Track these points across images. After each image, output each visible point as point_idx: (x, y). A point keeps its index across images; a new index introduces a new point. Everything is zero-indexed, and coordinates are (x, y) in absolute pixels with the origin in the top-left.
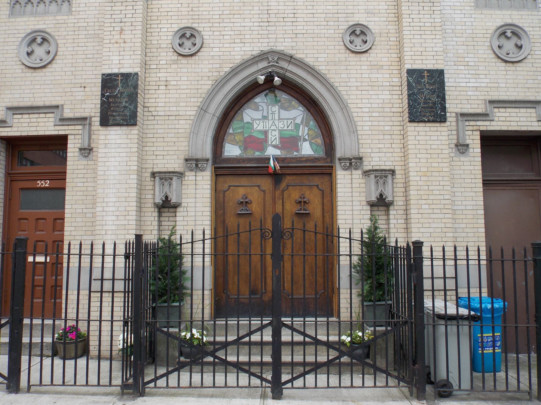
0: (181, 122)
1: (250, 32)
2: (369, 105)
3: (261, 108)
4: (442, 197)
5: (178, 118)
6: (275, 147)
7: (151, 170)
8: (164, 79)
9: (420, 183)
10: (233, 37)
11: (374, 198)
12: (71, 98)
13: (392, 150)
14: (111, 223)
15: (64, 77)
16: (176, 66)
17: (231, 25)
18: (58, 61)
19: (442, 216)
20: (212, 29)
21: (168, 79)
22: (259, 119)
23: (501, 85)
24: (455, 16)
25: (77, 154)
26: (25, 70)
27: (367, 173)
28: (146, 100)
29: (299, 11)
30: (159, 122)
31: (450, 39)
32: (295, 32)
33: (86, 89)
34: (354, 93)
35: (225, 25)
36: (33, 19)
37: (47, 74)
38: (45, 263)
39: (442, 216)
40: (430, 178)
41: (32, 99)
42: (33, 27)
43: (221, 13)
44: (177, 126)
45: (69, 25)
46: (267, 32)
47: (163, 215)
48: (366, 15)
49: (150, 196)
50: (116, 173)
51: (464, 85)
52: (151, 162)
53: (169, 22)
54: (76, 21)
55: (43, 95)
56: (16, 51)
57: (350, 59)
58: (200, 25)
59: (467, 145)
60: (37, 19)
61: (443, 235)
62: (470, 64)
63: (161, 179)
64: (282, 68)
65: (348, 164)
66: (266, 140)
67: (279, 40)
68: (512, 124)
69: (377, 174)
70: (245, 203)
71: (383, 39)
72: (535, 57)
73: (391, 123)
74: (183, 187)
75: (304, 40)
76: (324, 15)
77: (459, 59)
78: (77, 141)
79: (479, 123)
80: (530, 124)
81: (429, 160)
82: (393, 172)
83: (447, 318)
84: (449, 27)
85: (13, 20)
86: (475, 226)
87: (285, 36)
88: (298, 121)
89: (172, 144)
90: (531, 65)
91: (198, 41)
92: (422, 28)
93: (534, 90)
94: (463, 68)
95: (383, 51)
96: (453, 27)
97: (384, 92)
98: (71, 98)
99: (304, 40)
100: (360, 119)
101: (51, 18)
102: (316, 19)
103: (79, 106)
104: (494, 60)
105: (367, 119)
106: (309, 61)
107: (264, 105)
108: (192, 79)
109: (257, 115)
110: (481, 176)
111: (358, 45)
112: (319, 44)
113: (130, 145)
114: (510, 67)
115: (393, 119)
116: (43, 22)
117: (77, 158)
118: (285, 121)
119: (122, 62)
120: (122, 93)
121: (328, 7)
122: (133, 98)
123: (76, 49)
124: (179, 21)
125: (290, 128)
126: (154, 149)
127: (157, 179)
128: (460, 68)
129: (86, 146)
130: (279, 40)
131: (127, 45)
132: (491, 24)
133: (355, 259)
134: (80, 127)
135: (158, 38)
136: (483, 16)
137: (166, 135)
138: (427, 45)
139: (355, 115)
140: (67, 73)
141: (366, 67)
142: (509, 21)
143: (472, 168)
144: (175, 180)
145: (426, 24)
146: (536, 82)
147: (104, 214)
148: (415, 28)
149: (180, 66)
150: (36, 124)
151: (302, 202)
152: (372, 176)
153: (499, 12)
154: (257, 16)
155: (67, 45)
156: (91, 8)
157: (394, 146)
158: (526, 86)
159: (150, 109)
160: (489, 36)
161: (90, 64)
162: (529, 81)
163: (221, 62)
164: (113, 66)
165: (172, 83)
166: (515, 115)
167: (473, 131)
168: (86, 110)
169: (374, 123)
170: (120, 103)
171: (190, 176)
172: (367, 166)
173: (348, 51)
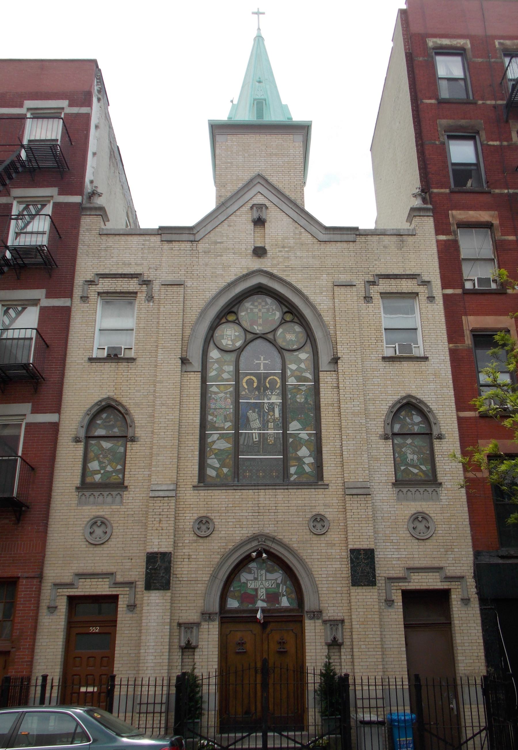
0: (199, 585)
1: (246, 520)
2: (326, 572)
3: (253, 572)
4: (374, 640)
5: (197, 582)
6: (263, 600)
7: (177, 621)
8: (187, 554)
9: (360, 630)
10: (235, 523)
11: (329, 641)
12: (121, 567)
13: (342, 605)
14: (151, 661)
15: (117, 552)
16: (195, 544)
17: (234, 514)
18: (113, 540)
19: (374, 653)
20: (221, 517)
21: (191, 554)
22: (251, 580)
23: (415, 556)
24: (384, 507)
25: (125, 609)
26: (88, 546)
27: (325, 622)
28: (175, 570)
29: (279, 505)
30: (184, 585)
31: (380, 523)
32: (276, 520)
33: (133, 561)
34: (316, 563)
35: (229, 514)
36: (95, 507)
37: (105, 549)
38: (93, 693)
39: (374, 653)
40: (366, 626)
41: (93, 568)
42: (94, 514)
43: (226, 506)
44: (196, 588)
45: (121, 513)
46: (257, 520)
47: (185, 654)
48: (323, 507)
49: (177, 640)
50: (155, 624)
51: (390, 556)
52: (178, 615)
53: (192, 512)
54: (126, 510)
55: (101, 564)
56: (82, 531)
57: (313, 539)
58: (213, 514)
59: (393, 601)
60: (98, 507)
61: (376, 667)
62: (394, 541)
63: (185, 628)
64: (268, 546)
65: (312, 616)
66: (256, 596)
67: (265, 526)
68: (423, 584)
69: (332, 623)
70: (241, 644)
71: (335, 524)
72: (438, 535)
73: (341, 585)
74: (200, 633)
75: (282, 525)
76: (296, 508)
77: (386, 538)
78: (125, 599)
79: (400, 584)
80: (435, 584)
81: (366, 613)
82: (342, 621)
83: (370, 723)
84: (379, 515)
85: (80, 508)
86: (400, 659)
87: (270, 523)
88: (279, 581)
89: (193, 601)
90: (435, 541)
91: (211, 526)
92: (360, 519)
93: (438, 559)
94: (389, 544)
95: (335, 533)
96: (382, 515)
97: (336, 563)
98: (121, 567)
99: (282, 525)
100: (320, 582)
101: (108, 507)
102: (290, 511)
103: (127, 573)
104: (410, 538)
105: (325, 582)
106: (286, 541)
107: (255, 570)
108: (207, 554)
109: (250, 577)
110: (403, 623)
111: (319, 528)
112: (293, 528)
113: (165, 604)
114: (422, 543)
115: (342, 582)
116: (102, 510)
117: (125, 612)
118: (270, 581)
119: (160, 543)
120: (160, 567)
121: (299, 502)
122: (168, 570)
123: (125, 530)
124: (198, 512)
125: (273, 586)
126: (180, 605)
127: (183, 628)
128: (387, 544)
129: (132, 602)
130: (265, 526)
131: (164, 531)
132: (408, 512)
133: (317, 685)
134: (128, 589)
135: (183, 524)
136: (402, 506)
137: (188, 595)
138: (363, 531)
139: (317, 579)
140: (119, 549)
141: (324, 545)
142: (420, 510)
143: (396, 617)
144: (195, 630)
145: (363, 516)
146: (439, 553)
147: (146, 654)
148: (355, 519)
149: (199, 544)
150: (96, 586)
151: (282, 643)
152: (328, 625)
153: (413, 503)
154: (251, 508)
155: (119, 528)
156: (137, 501)
157: (343, 601)
158: (433, 556)
159: (178, 576)
160: (406, 520)
161: (136, 542)
162: (434, 553)
163: (226, 541)
164: (154, 547)
165: (193, 557)
166: (425, 577)
167: (396, 590)
168: (133, 576)
169: (330, 585)
170: (159, 574)
171: (205, 626)
172: (326, 617)
173: (312, 533)
